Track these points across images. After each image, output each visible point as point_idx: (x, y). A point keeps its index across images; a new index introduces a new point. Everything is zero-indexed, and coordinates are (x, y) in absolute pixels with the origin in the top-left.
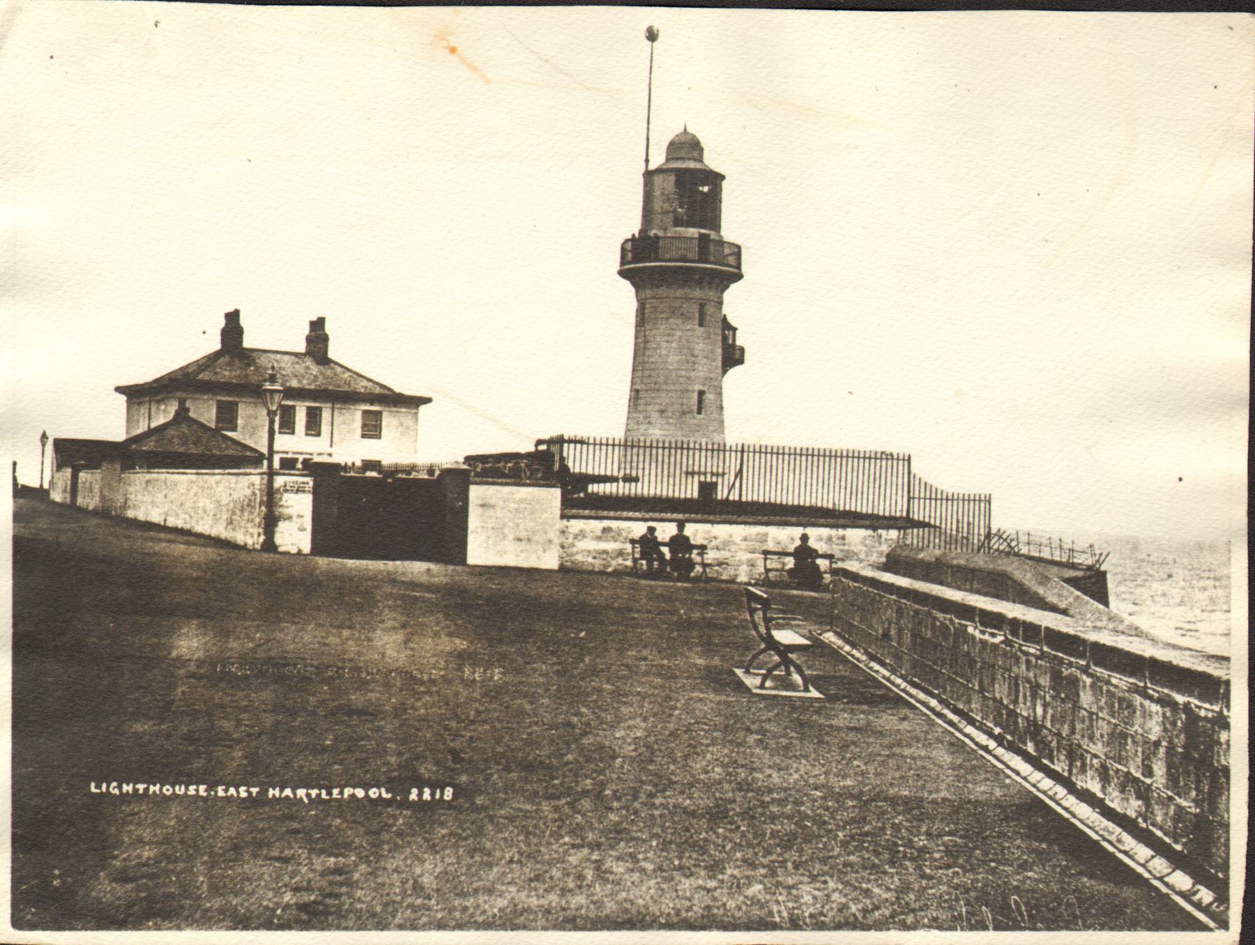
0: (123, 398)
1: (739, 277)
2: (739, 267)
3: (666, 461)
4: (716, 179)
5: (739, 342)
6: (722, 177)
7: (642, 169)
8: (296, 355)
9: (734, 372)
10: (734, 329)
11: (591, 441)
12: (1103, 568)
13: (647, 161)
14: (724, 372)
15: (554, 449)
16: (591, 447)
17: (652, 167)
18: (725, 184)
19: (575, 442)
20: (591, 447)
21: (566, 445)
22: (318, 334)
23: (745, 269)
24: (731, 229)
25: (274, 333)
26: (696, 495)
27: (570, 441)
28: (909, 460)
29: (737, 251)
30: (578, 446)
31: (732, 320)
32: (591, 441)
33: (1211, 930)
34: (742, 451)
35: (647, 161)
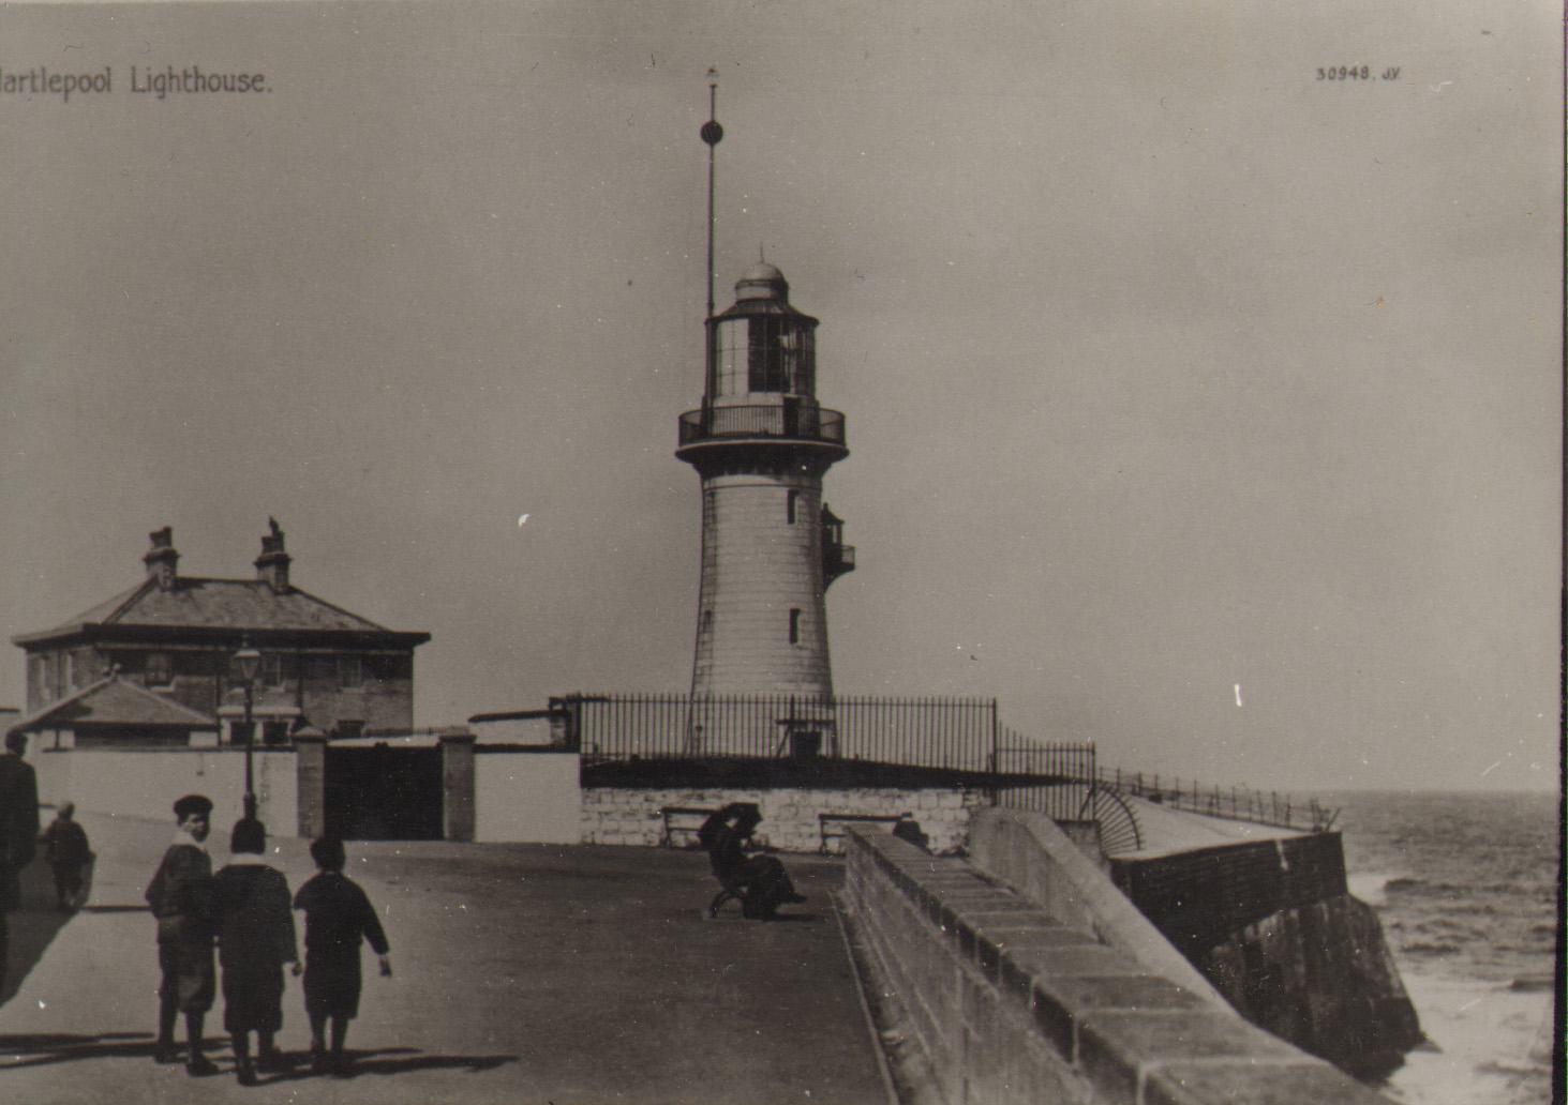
0: (22, 652)
1: (841, 453)
2: (841, 439)
3: (724, 715)
4: (807, 324)
5: (847, 541)
6: (814, 322)
7: (704, 315)
8: (246, 583)
9: (841, 584)
10: (839, 523)
11: (613, 698)
12: (1334, 828)
13: (711, 305)
14: (826, 583)
15: (571, 708)
16: (613, 705)
17: (718, 312)
18: (819, 332)
19: (595, 700)
20: (613, 705)
21: (584, 706)
22: (274, 555)
23: (850, 444)
24: (828, 394)
25: (220, 554)
26: (787, 751)
27: (588, 700)
28: (994, 706)
29: (840, 422)
30: (598, 705)
31: (837, 510)
32: (613, 698)
33: (476, 719)
34: (771, 703)
35: (711, 305)
